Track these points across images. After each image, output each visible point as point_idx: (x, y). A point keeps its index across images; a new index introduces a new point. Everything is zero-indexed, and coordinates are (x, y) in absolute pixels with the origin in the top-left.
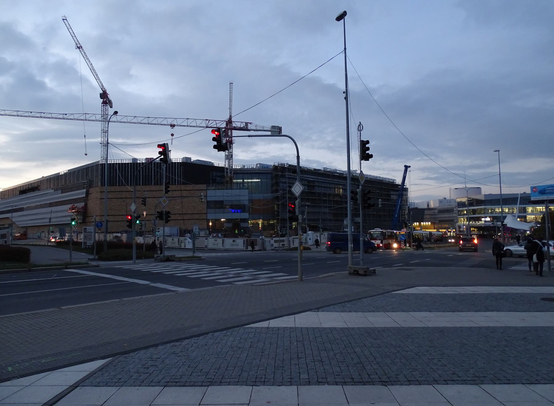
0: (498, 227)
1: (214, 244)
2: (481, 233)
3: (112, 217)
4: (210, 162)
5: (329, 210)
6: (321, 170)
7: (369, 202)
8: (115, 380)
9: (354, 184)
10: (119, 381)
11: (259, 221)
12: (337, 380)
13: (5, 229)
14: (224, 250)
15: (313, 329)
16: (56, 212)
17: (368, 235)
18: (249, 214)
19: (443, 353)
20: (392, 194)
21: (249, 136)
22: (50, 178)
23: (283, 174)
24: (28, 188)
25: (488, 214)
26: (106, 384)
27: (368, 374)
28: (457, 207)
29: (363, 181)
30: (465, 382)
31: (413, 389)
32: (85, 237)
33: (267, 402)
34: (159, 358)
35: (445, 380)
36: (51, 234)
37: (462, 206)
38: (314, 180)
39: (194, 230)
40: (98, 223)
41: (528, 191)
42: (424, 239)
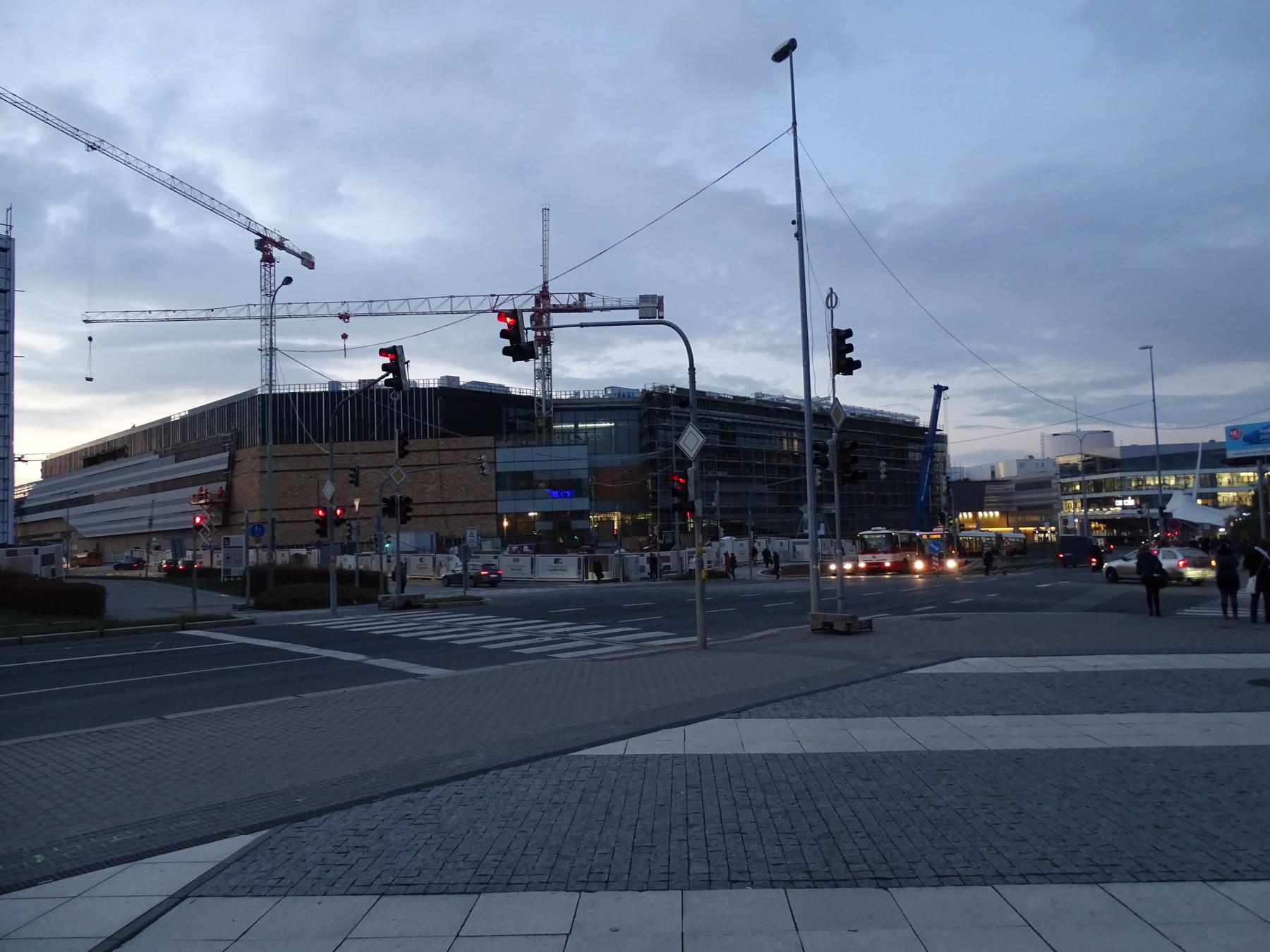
0: (1151, 519)
1: (512, 568)
2: (1115, 535)
3: (287, 512)
4: (501, 386)
5: (769, 487)
6: (749, 399)
7: (853, 468)
8: (271, 881)
9: (824, 429)
10: (279, 884)
11: (612, 516)
12: (775, 877)
13: (51, 543)
15: (726, 757)
16: (164, 504)
17: (857, 541)
18: (591, 500)
19: (1020, 811)
20: (912, 450)
21: (582, 325)
22: (150, 430)
23: (665, 409)
24: (103, 451)
25: (1129, 490)
26: (250, 892)
27: (845, 862)
28: (1059, 476)
29: (841, 421)
30: (1067, 878)
31: (949, 894)
32: (227, 558)
33: (611, 930)
34: (374, 829)
35: (1024, 873)
36: (155, 552)
37: (1069, 475)
38: (734, 420)
39: (468, 538)
40: (255, 526)
41: (1219, 435)
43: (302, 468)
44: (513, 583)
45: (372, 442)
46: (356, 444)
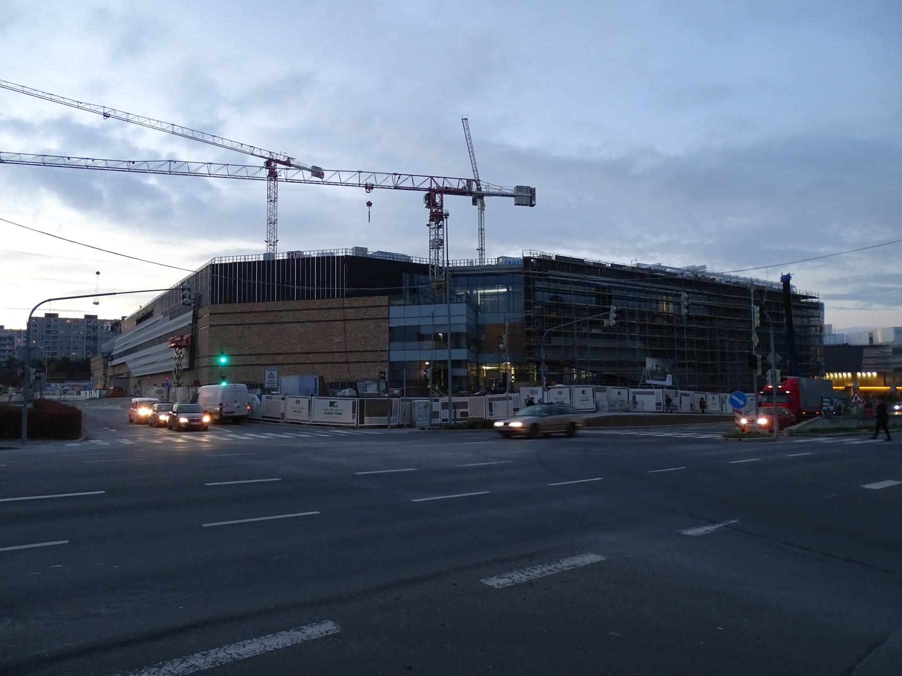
9: (698, 294)
14: (311, 425)
38: (610, 284)
42: (824, 404)
43: (240, 323)
44: (296, 425)
45: (292, 301)
46: (281, 303)
